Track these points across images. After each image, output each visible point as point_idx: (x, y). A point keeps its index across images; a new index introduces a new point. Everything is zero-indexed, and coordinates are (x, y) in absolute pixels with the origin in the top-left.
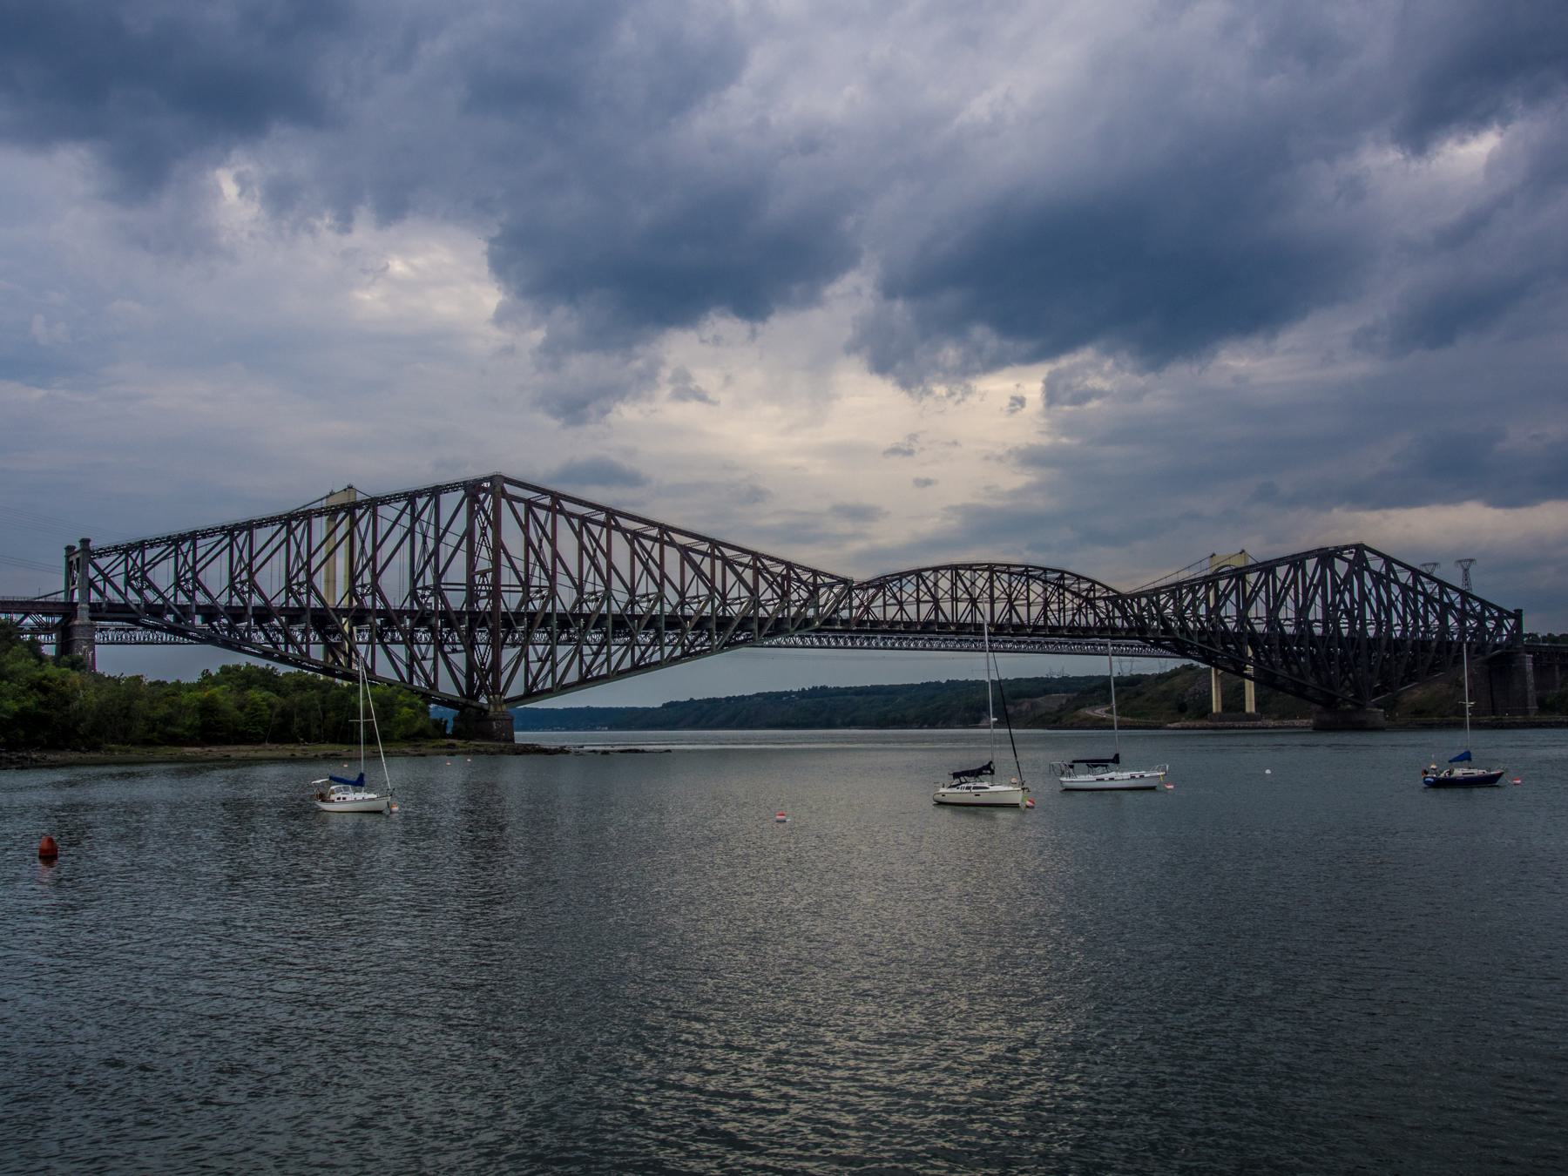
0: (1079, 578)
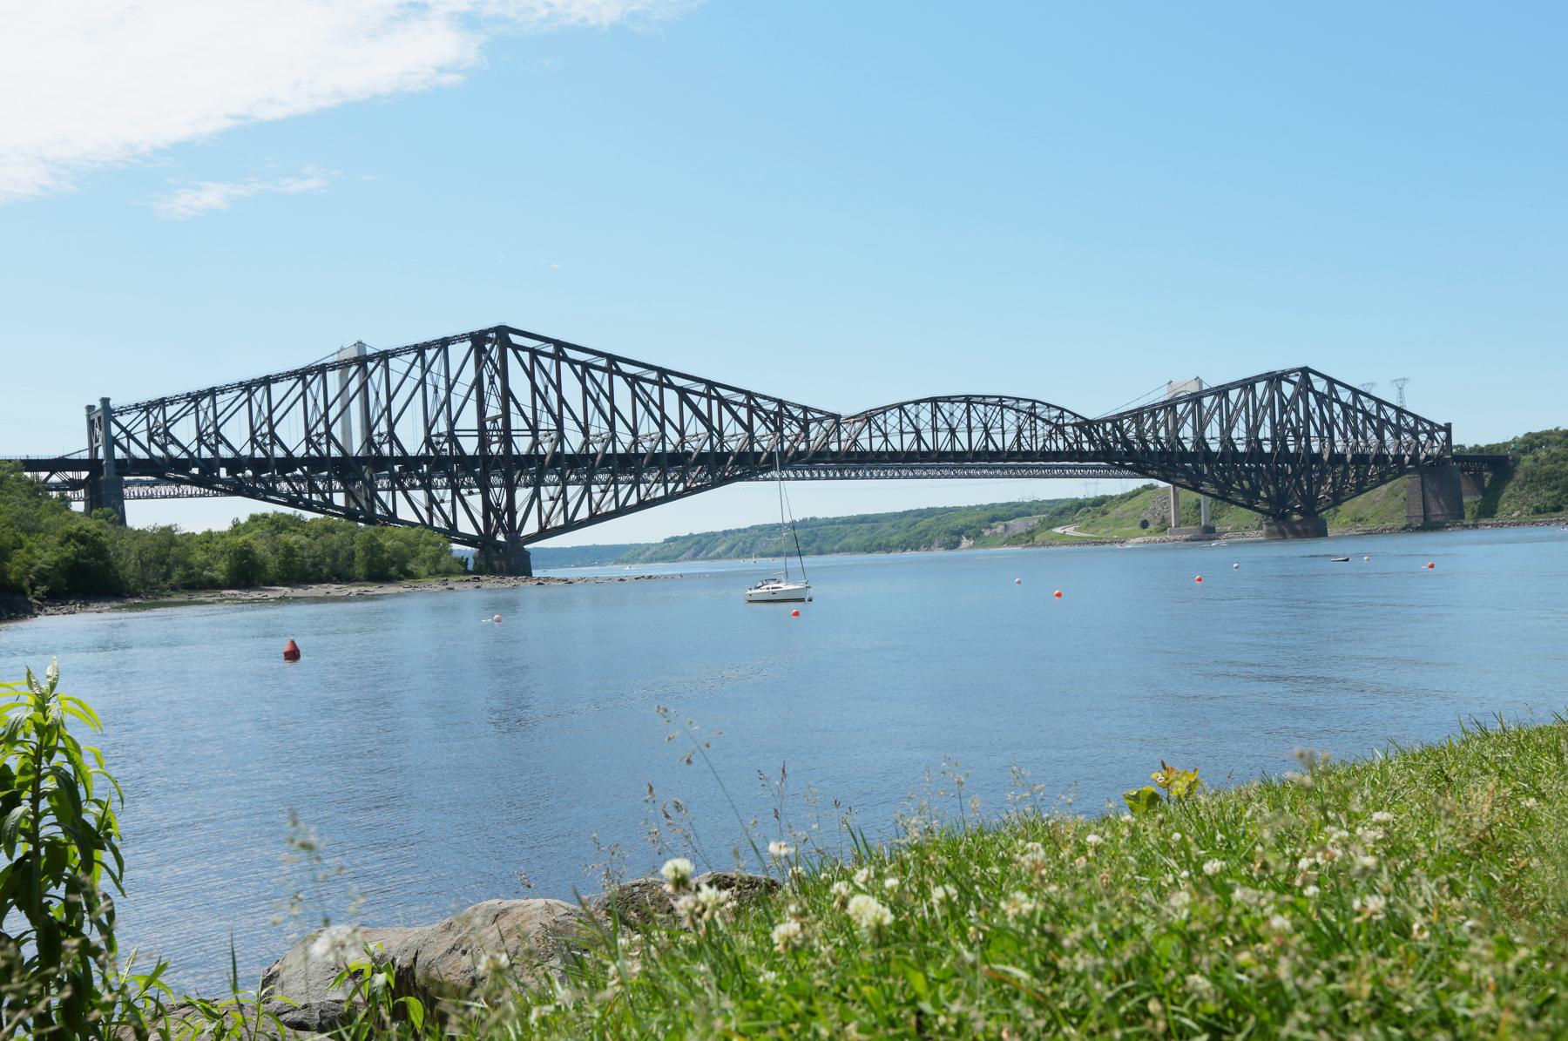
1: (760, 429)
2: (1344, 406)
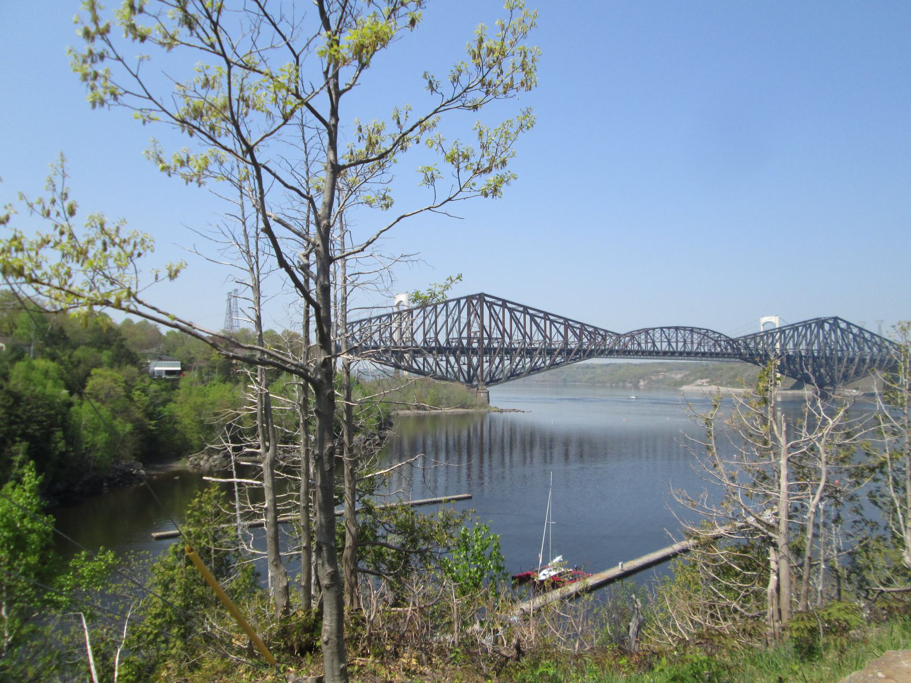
0: (714, 332)
1: (571, 338)
2: (854, 335)
